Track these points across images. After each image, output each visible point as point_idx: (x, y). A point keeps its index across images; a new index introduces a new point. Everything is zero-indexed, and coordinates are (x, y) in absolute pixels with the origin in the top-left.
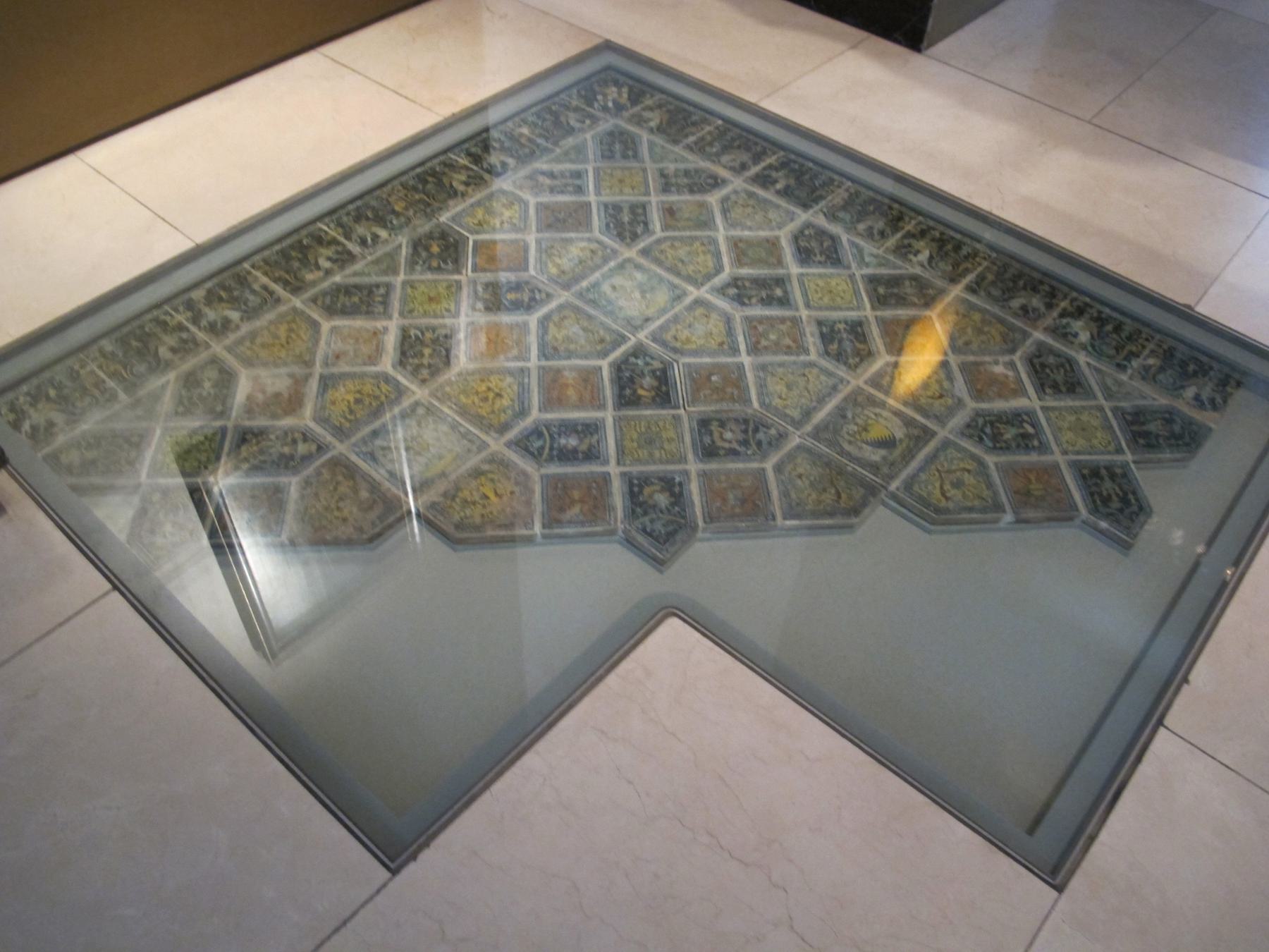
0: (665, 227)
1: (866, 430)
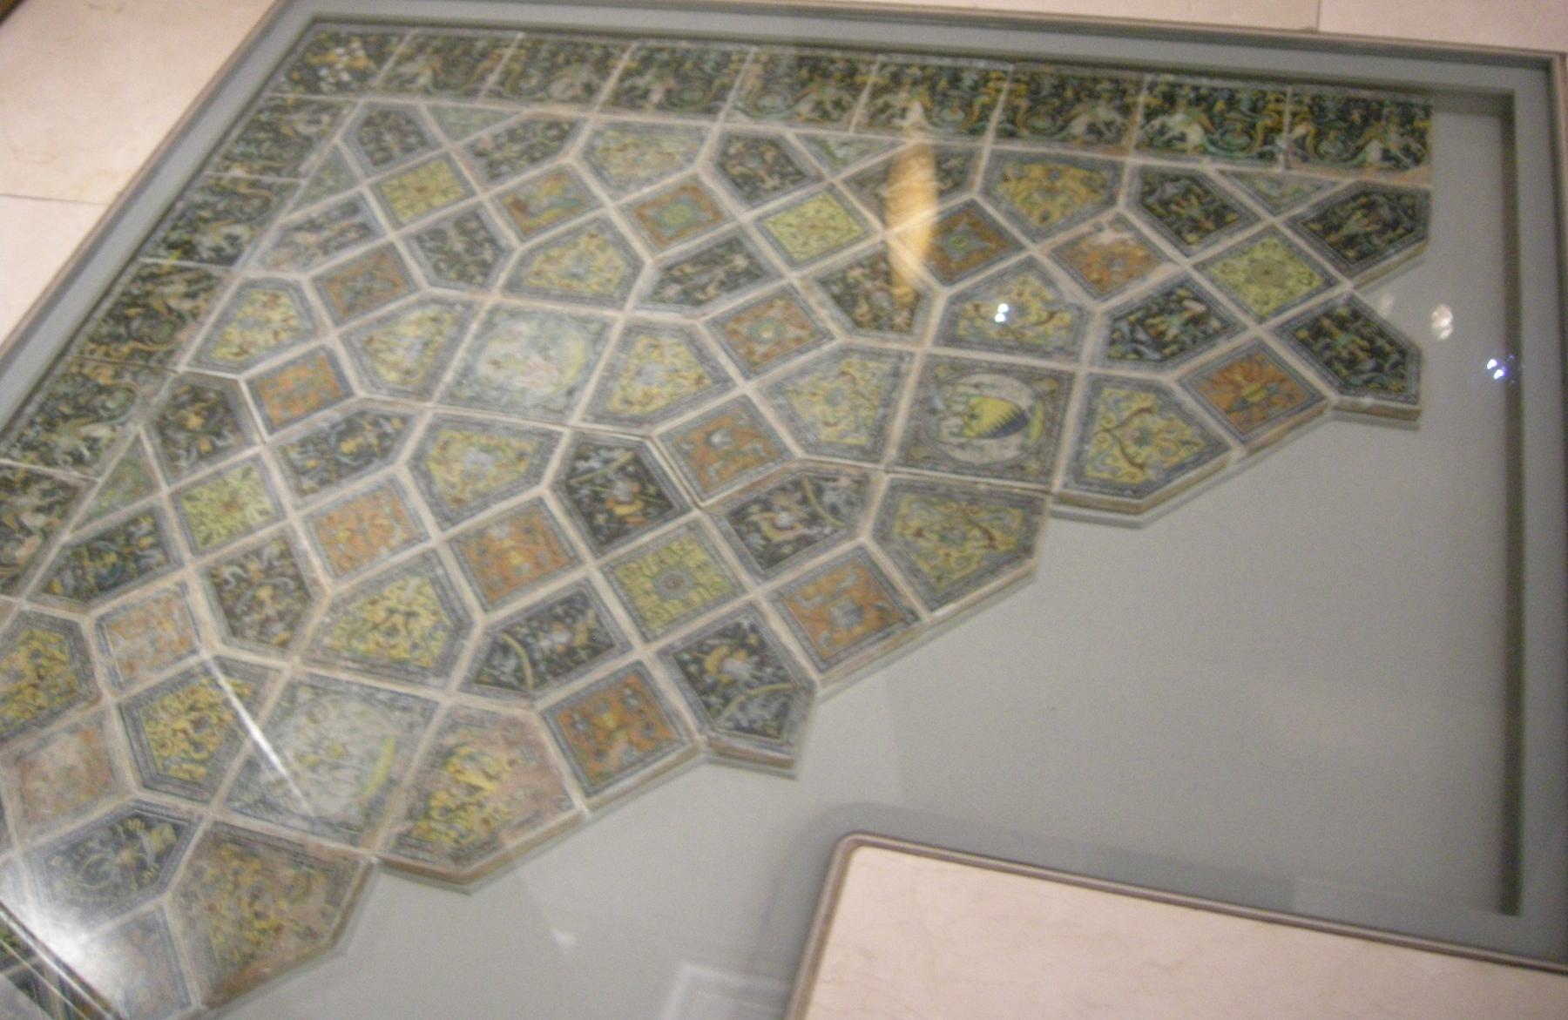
0: (525, 234)
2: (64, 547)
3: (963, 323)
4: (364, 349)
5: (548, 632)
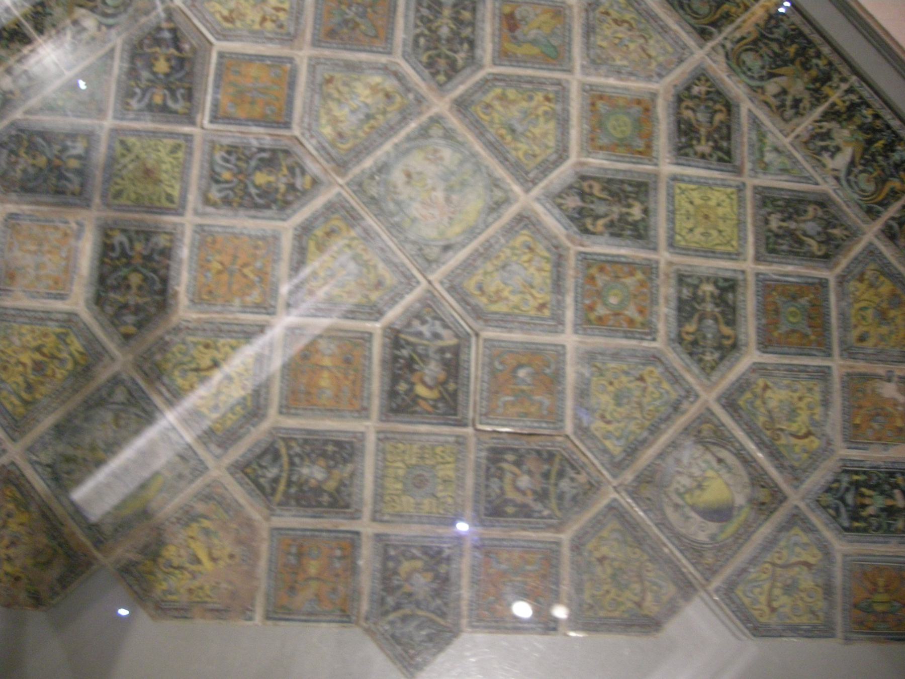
0: (503, 56)
1: (700, 486)
2: (13, 124)
3: (748, 395)
4: (321, 85)
5: (313, 463)
